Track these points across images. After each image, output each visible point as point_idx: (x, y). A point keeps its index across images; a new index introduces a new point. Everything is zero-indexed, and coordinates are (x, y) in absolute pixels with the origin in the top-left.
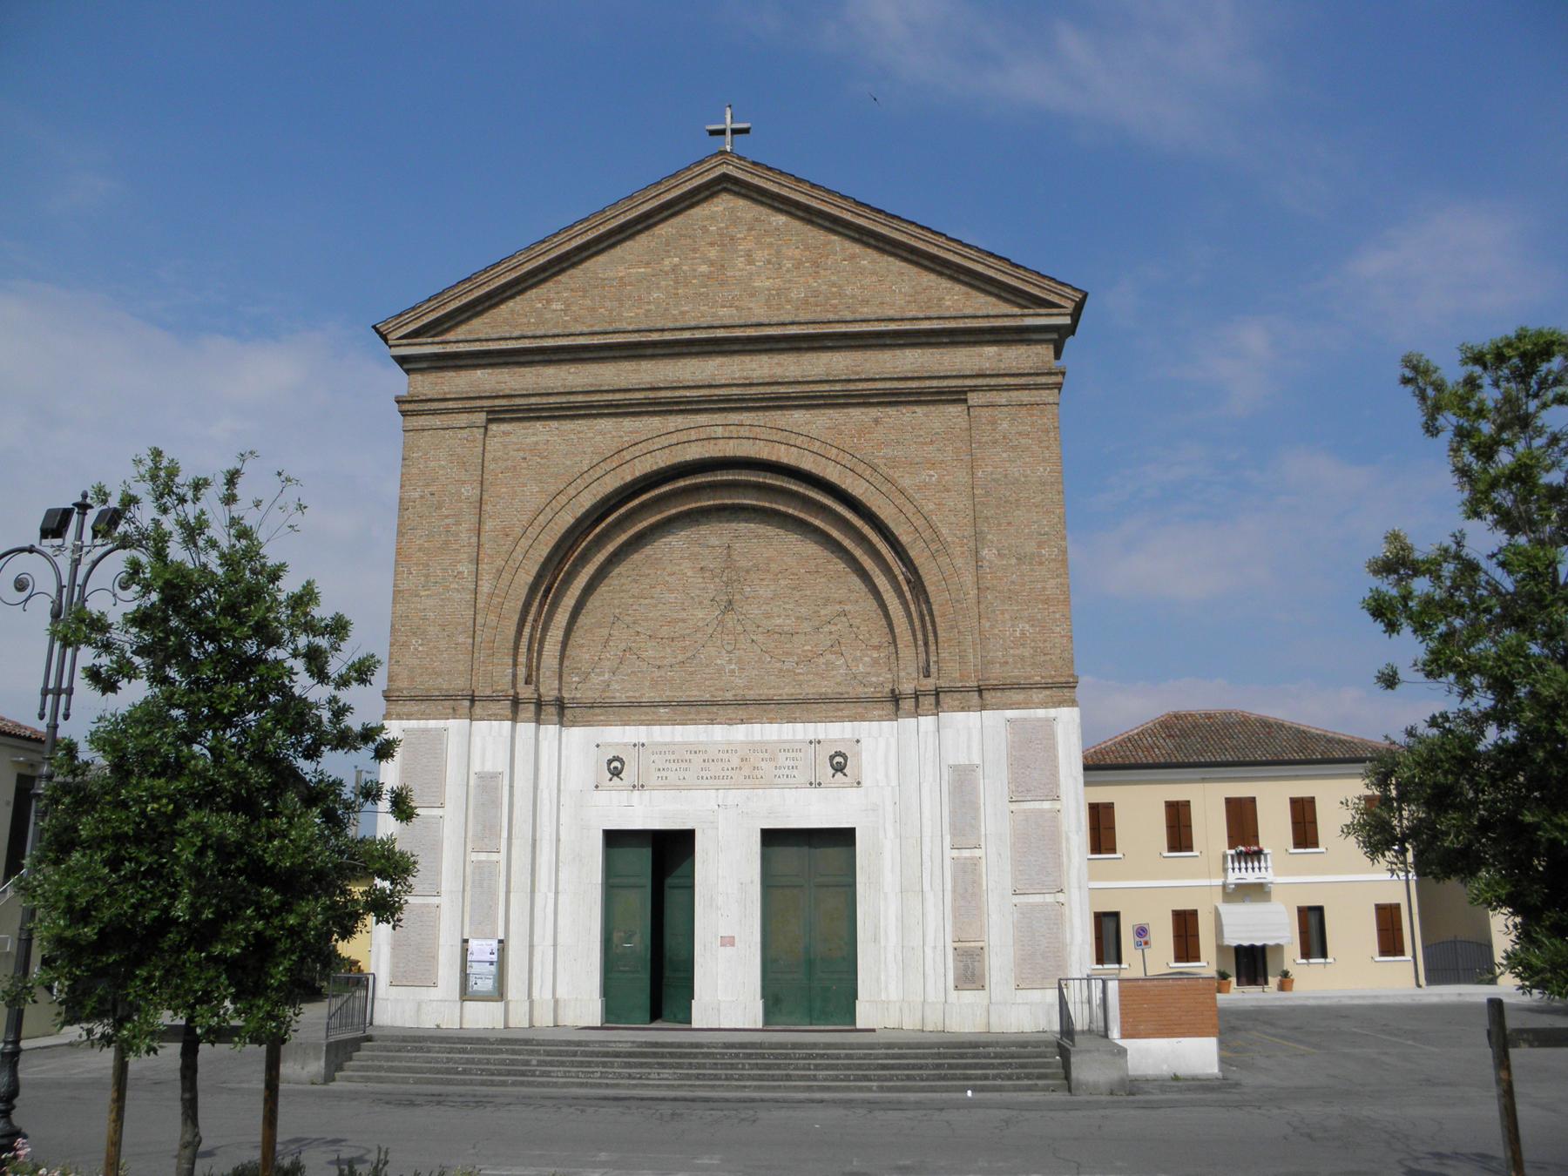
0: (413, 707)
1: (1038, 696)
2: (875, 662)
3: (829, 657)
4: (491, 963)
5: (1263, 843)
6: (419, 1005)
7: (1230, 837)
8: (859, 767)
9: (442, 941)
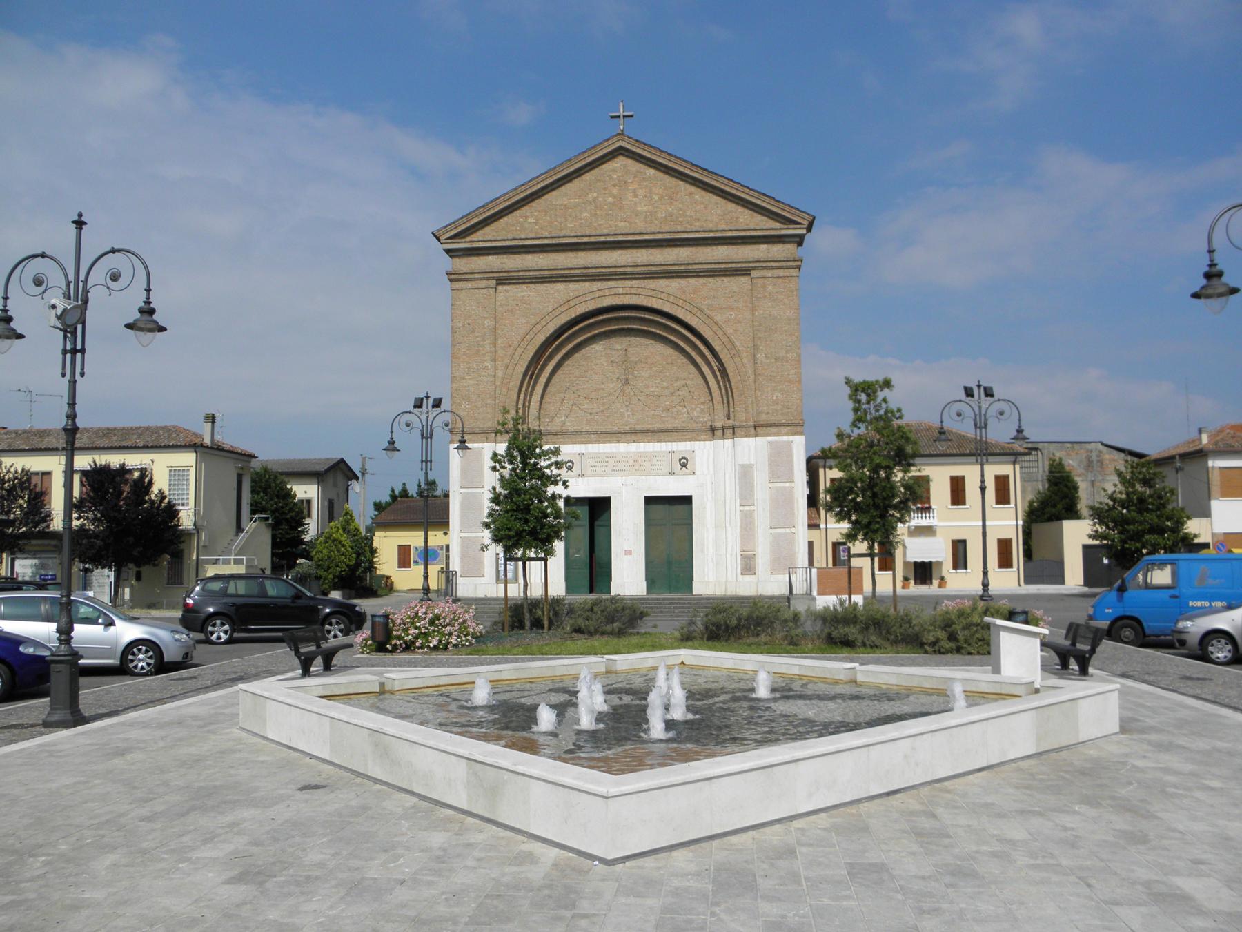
1: (784, 430)
2: (702, 411)
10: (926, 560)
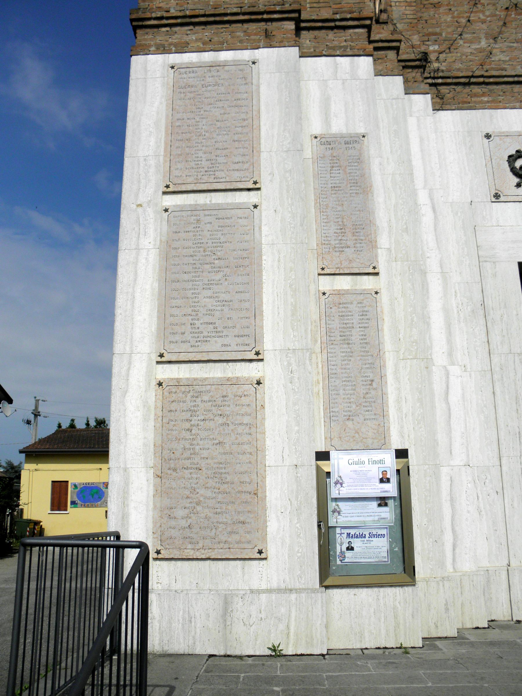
0: (191, 35)
4: (383, 501)
6: (227, 602)
9: (271, 457)
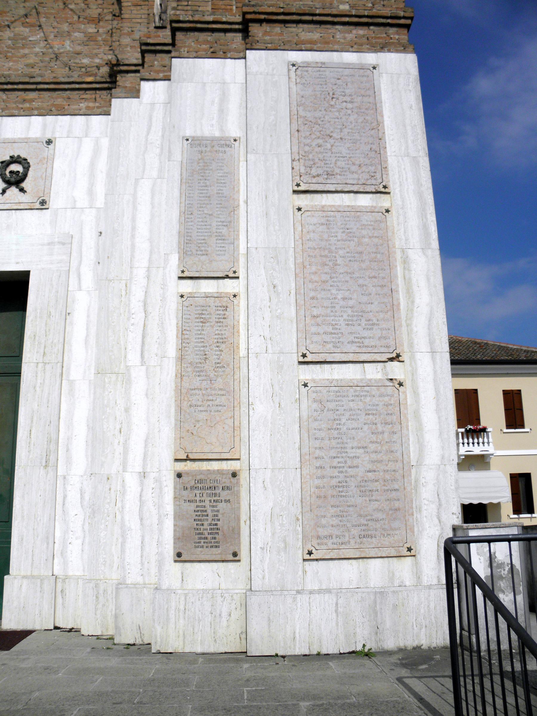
1: (340, 33)
2: (91, 39)
3: (20, 29)
5: (483, 423)
7: (459, 420)
8: (48, 178)
10: (475, 502)
